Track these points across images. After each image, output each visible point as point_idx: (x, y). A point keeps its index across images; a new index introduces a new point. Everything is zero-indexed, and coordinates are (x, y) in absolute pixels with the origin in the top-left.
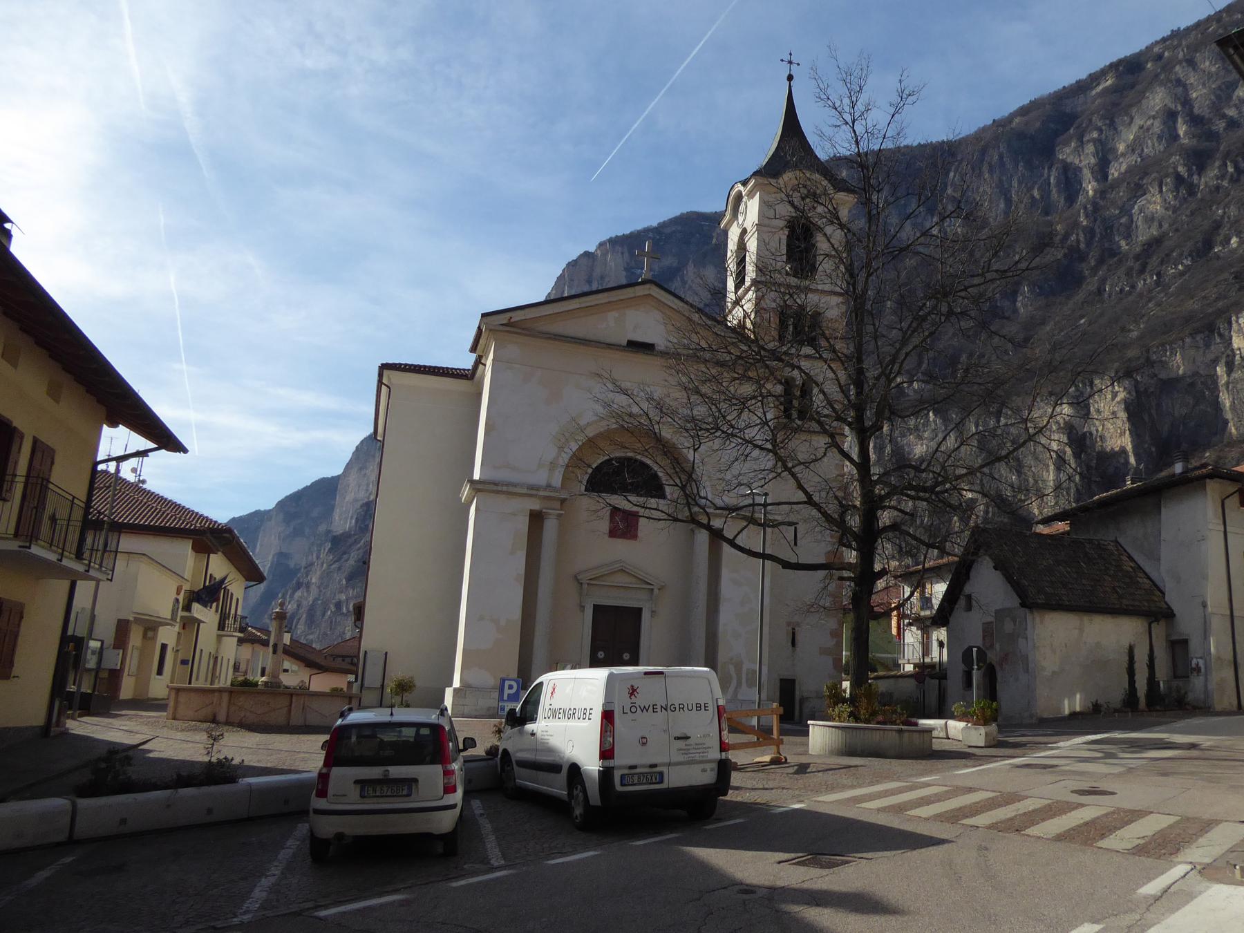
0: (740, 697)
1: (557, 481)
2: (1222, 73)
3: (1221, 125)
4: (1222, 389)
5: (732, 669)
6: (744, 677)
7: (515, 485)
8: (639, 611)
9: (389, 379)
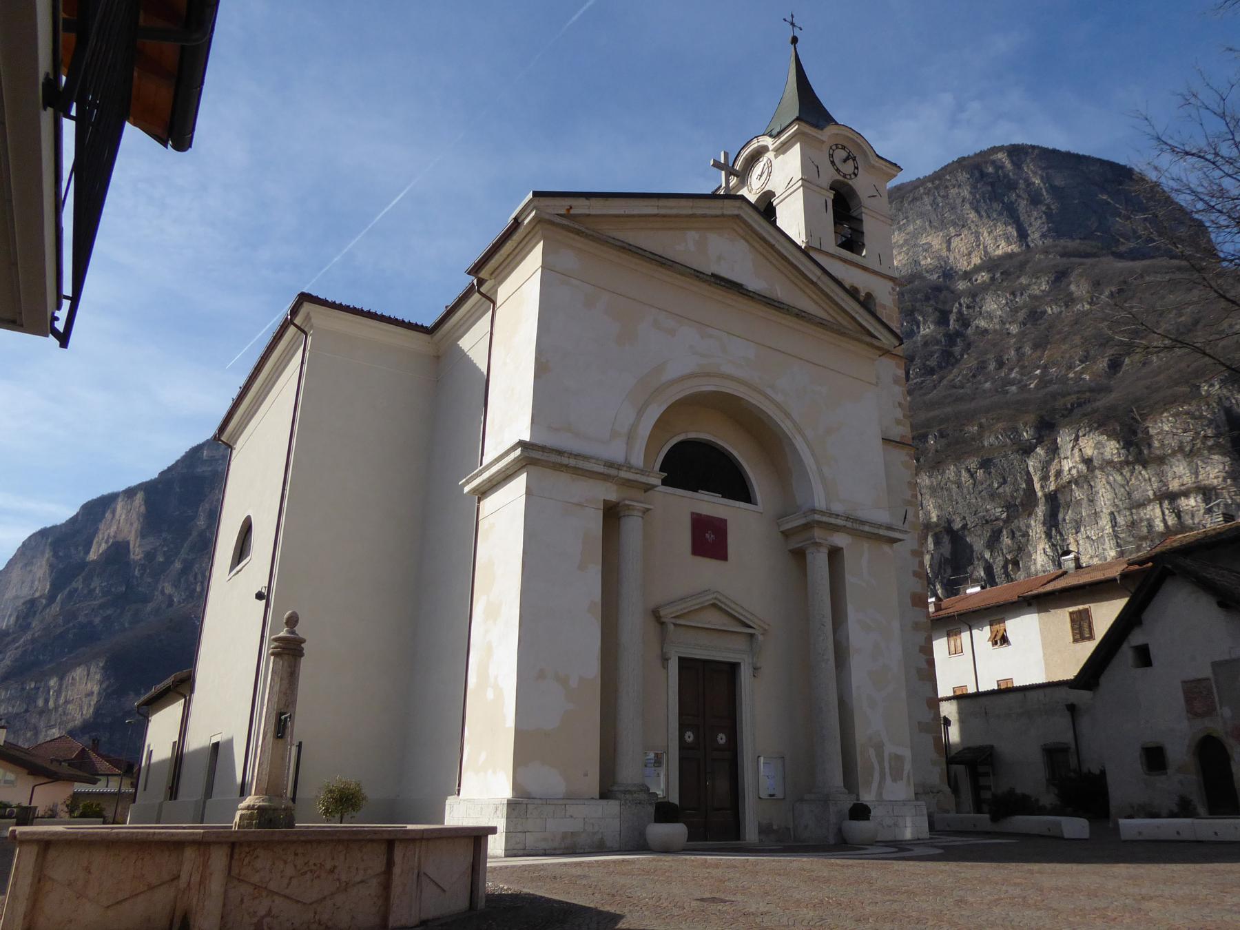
0: (886, 797)
1: (638, 459)
5: (872, 752)
6: (887, 765)
7: (586, 458)
8: (733, 668)
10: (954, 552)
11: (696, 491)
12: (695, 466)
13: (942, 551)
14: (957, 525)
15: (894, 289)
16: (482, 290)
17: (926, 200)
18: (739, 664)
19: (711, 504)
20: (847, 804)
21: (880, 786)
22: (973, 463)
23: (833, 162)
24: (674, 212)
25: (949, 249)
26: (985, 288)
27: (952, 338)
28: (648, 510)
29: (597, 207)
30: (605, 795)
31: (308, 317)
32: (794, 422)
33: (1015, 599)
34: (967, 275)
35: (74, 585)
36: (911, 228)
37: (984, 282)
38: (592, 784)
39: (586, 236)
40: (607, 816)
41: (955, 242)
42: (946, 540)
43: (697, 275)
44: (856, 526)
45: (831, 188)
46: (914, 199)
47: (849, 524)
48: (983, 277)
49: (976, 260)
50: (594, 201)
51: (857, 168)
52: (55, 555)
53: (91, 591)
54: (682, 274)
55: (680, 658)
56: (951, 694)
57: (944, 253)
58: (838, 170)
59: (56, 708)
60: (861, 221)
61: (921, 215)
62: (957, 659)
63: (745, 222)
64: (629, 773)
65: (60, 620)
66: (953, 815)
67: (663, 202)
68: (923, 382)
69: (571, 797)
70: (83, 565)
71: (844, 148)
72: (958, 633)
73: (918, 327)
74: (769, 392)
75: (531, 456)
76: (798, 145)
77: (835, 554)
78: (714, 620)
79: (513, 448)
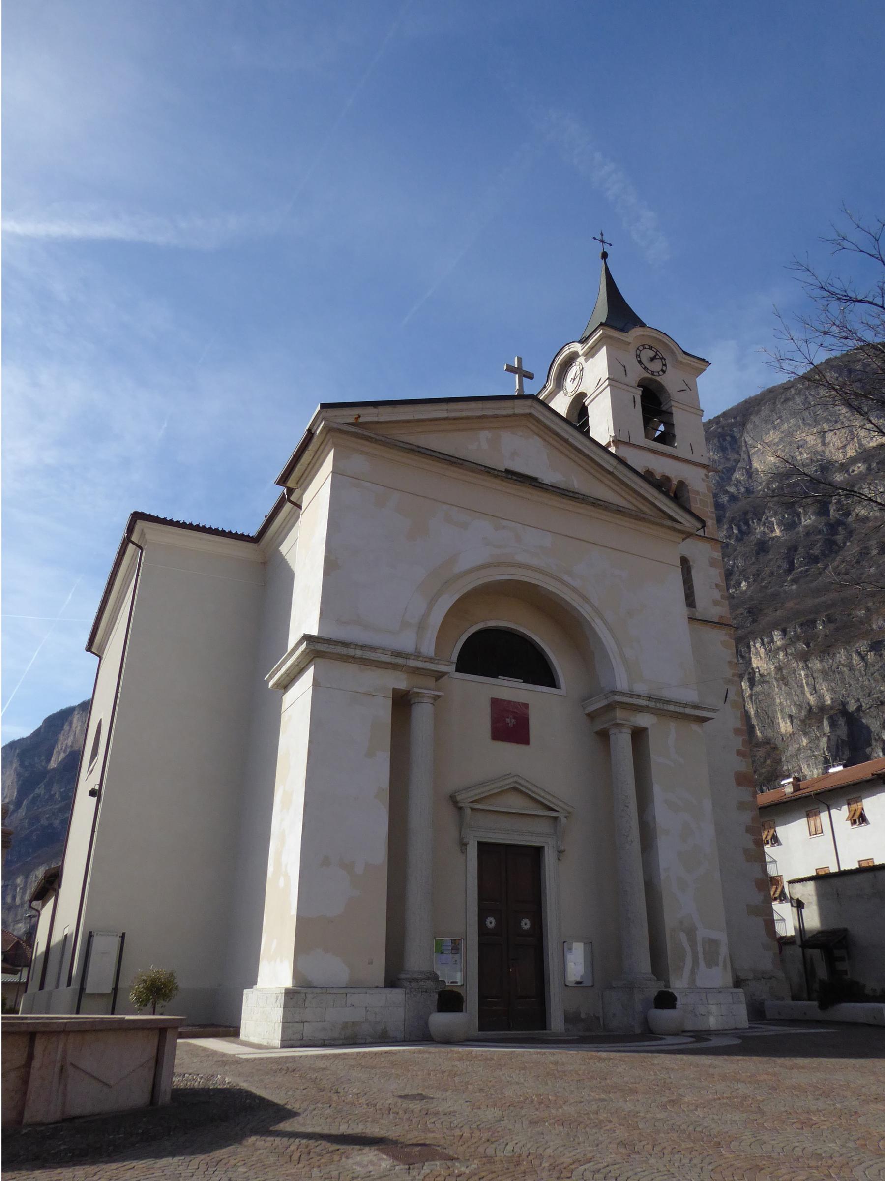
1: (429, 648)
2: (723, 461)
3: (725, 499)
4: (747, 700)
5: (683, 938)
6: (700, 949)
8: (537, 852)
9: (142, 534)
10: (851, 734)
11: (497, 677)
12: (495, 653)
13: (839, 733)
14: (852, 707)
15: (707, 476)
16: (292, 499)
17: (799, 400)
18: (543, 847)
19: (511, 689)
20: (653, 989)
21: (693, 972)
22: (863, 646)
23: (640, 362)
24: (464, 414)
25: (824, 444)
26: (862, 477)
27: (833, 527)
28: (439, 697)
29: (385, 415)
30: (392, 982)
31: (142, 534)
32: (592, 606)
33: (869, 777)
34: (844, 467)
35: (37, 791)
36: (785, 427)
37: (861, 472)
38: (378, 971)
39: (376, 441)
40: (391, 1006)
41: (829, 436)
42: (842, 722)
43: (489, 471)
44: (659, 706)
45: (639, 386)
46: (787, 400)
47: (652, 704)
48: (859, 468)
49: (851, 453)
50: (381, 409)
51: (665, 365)
52: (22, 764)
53: (52, 797)
54: (473, 471)
55: (479, 843)
56: (814, 874)
57: (819, 448)
58: (645, 369)
59: (22, 904)
60: (671, 414)
61: (794, 414)
62: (818, 839)
63: (538, 421)
64: (418, 958)
65: (26, 825)
66: (789, 1002)
67: (452, 406)
68: (807, 571)
69: (354, 986)
70: (45, 772)
71: (651, 348)
72: (817, 813)
73: (800, 520)
74: (566, 578)
75: (317, 648)
76: (605, 347)
77: (639, 735)
78: (516, 803)
79: (300, 643)
